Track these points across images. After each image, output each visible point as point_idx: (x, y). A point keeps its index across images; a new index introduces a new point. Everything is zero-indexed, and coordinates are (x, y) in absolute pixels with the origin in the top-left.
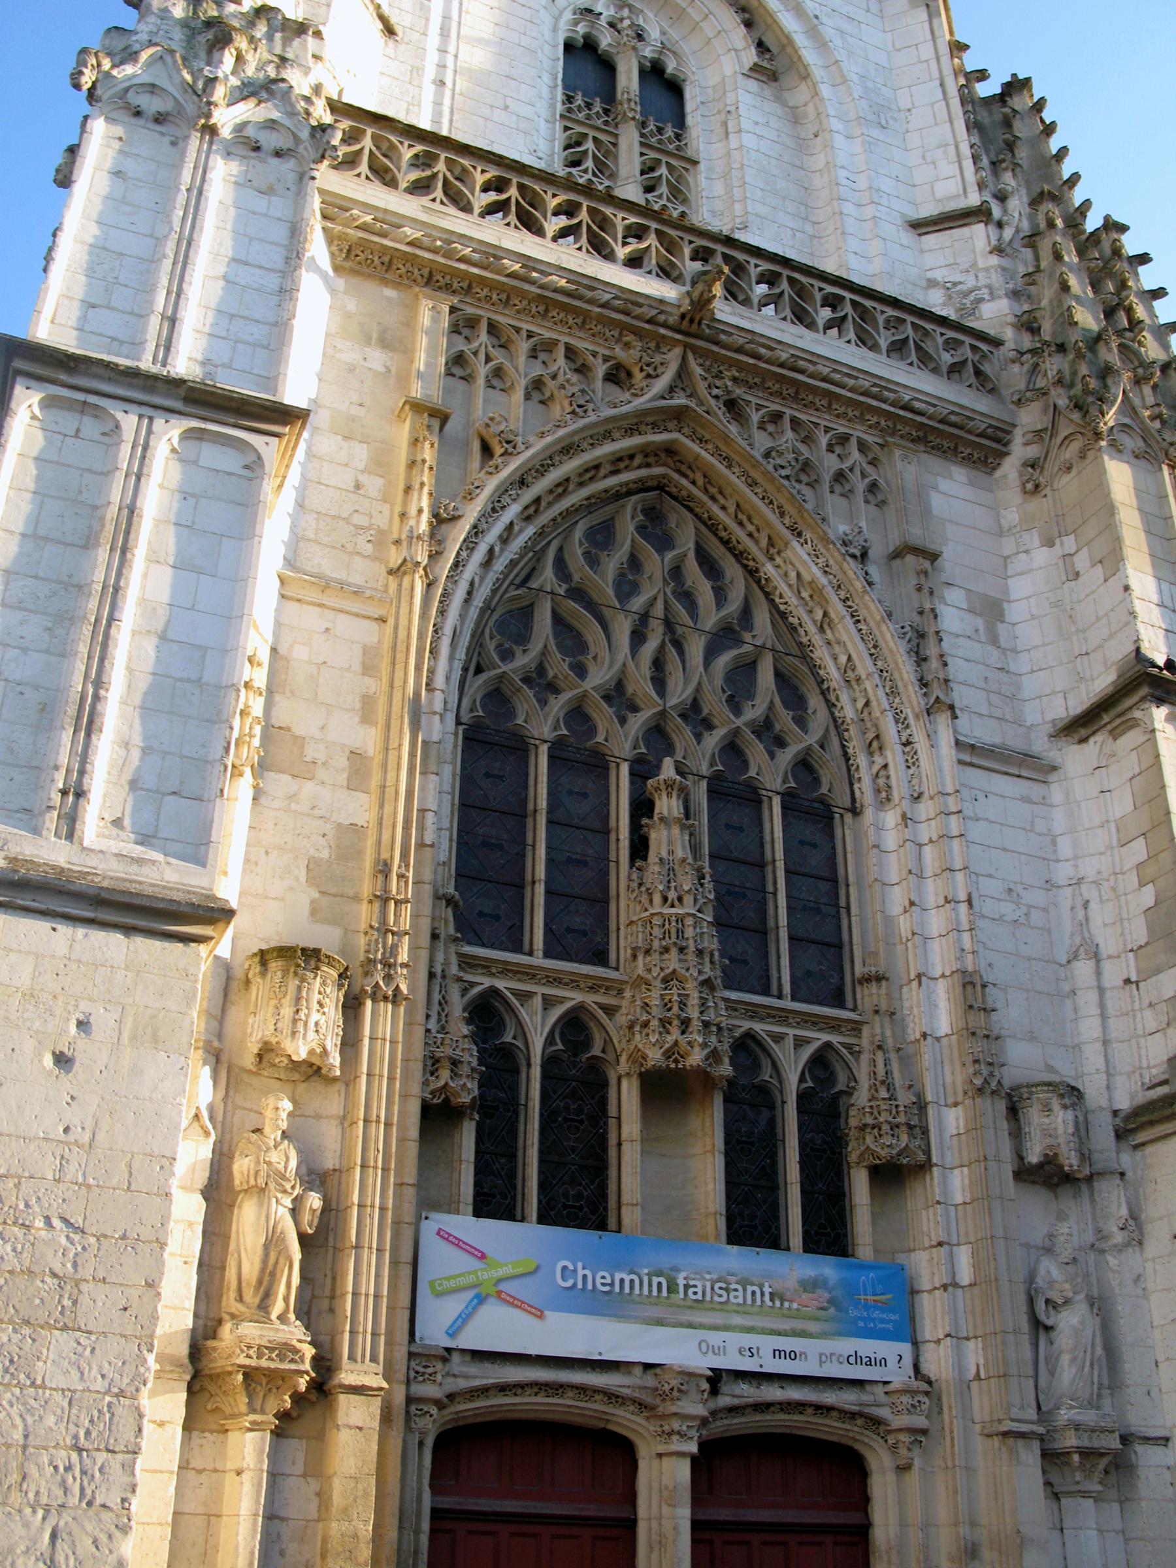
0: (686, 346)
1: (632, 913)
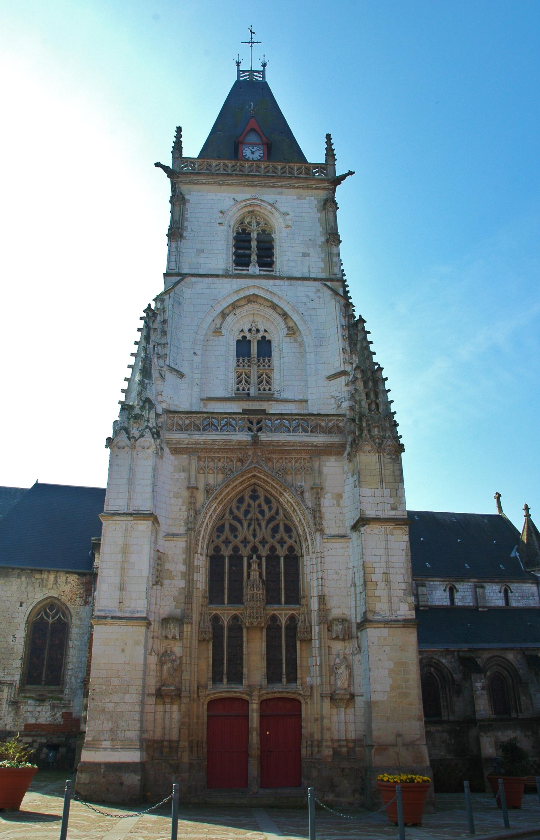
1: (247, 592)
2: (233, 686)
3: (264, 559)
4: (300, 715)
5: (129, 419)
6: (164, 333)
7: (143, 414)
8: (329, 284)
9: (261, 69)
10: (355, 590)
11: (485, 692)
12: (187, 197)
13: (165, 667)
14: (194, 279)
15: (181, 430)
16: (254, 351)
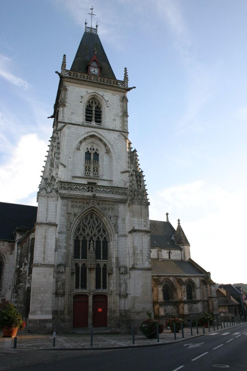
0: (93, 199)
1: (88, 255)
2: (83, 290)
3: (95, 242)
4: (107, 301)
5: (46, 184)
6: (59, 148)
7: (52, 182)
8: (123, 133)
9: (95, 28)
10: (129, 256)
11: (162, 292)
12: (68, 88)
13: (59, 283)
14: (70, 125)
15: (65, 189)
16: (92, 158)
